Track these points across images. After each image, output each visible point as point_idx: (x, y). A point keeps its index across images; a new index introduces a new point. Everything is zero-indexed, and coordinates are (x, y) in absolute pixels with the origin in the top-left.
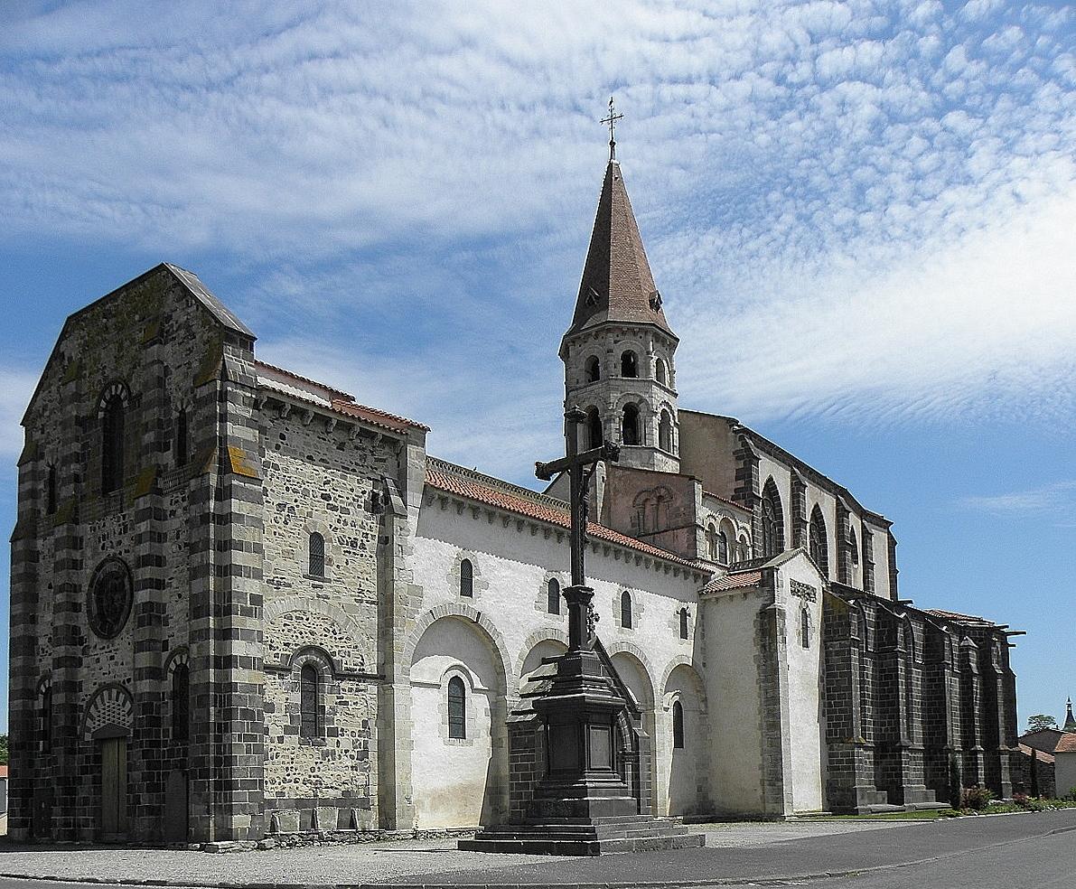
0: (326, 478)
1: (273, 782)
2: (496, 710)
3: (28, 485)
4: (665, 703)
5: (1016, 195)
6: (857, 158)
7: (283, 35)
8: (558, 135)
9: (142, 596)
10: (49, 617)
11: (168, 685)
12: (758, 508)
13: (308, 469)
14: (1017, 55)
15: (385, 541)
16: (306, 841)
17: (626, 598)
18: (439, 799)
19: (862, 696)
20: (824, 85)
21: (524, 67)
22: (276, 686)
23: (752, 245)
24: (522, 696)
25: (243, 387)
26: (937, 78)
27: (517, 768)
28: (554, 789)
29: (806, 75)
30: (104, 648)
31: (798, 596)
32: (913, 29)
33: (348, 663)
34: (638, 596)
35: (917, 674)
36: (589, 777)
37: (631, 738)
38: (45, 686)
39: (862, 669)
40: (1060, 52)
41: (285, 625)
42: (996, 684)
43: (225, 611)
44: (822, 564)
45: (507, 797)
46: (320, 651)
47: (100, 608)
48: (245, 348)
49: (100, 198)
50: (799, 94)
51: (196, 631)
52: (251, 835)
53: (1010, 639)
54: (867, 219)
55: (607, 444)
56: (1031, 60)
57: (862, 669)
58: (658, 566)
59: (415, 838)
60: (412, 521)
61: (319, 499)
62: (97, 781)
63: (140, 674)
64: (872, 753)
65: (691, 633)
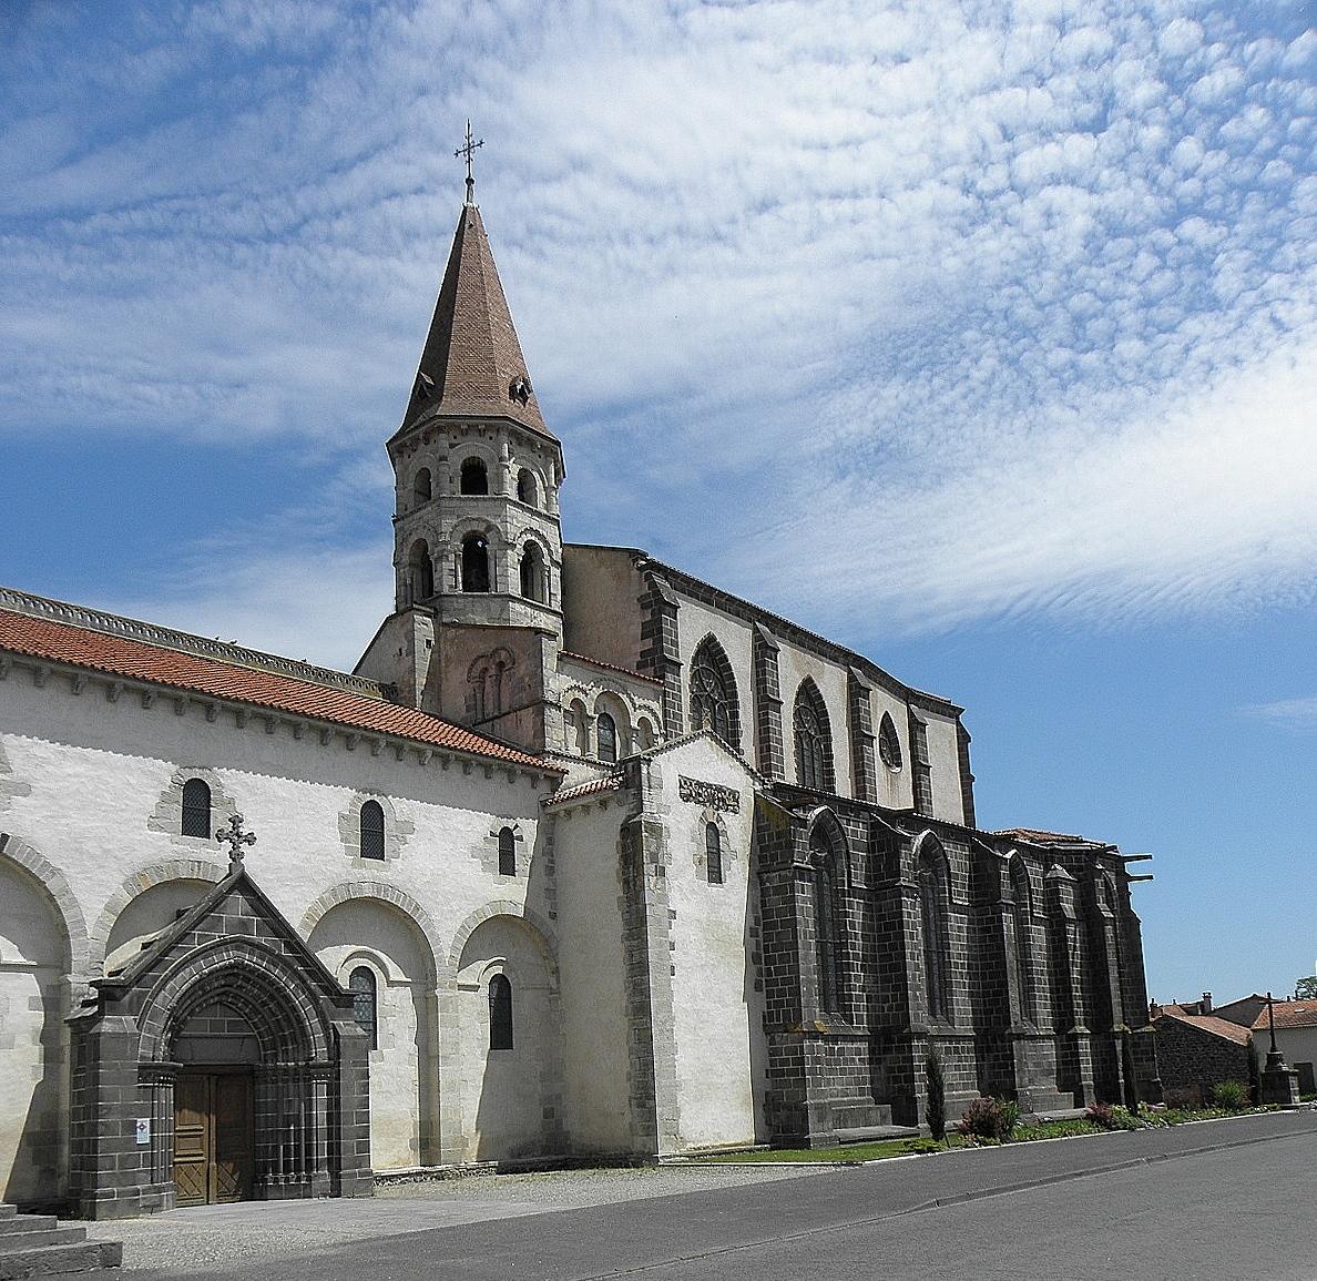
5: (1274, 320)
14: (1266, 143)
20: (1021, 191)
23: (946, 399)
26: (1166, 175)
32: (1130, 116)
34: (397, 809)
37: (327, 1037)
42: (1104, 934)
45: (66, 1149)
49: (145, 379)
50: (993, 204)
53: (1130, 868)
54: (1090, 359)
56: (1283, 148)
64: (864, 1045)
65: (522, 863)
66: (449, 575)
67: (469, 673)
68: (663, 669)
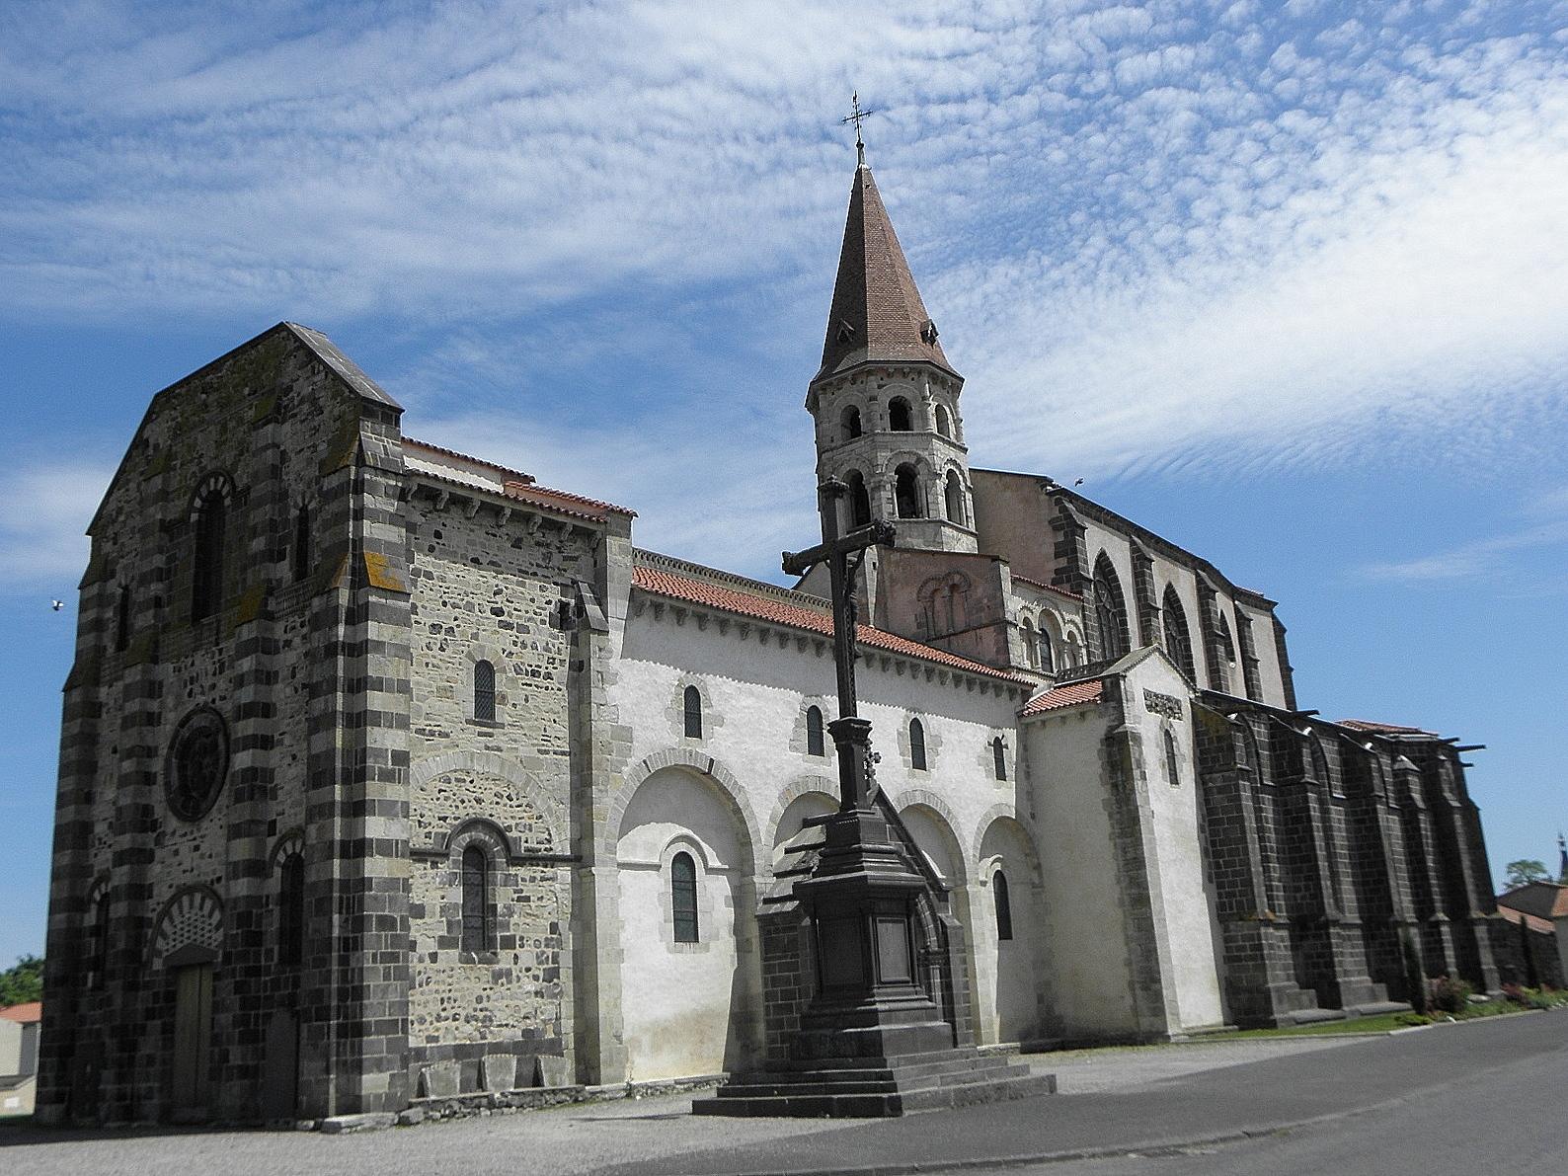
0: (497, 586)
1: (422, 1021)
2: (740, 897)
3: (91, 614)
4: (981, 873)
6: (1174, 168)
7: (471, 77)
8: (806, 166)
9: (242, 760)
10: (110, 794)
11: (274, 884)
12: (1089, 594)
13: (473, 575)
14: (1358, 49)
15: (579, 667)
16: (472, 1107)
17: (916, 728)
18: (664, 1034)
19: (1263, 849)
21: (762, 96)
22: (427, 880)
24: (778, 875)
25: (385, 473)
27: (775, 981)
28: (831, 1015)
29: (1103, 84)
30: (185, 835)
31: (1157, 712)
34: (932, 723)
35: (1337, 814)
36: (879, 995)
37: (936, 927)
38: (100, 891)
39: (1258, 810)
40: (1410, 43)
41: (440, 791)
43: (357, 775)
44: (1184, 664)
46: (490, 826)
47: (183, 777)
48: (390, 423)
49: (238, 265)
51: (315, 807)
52: (389, 1103)
53: (1464, 757)
54: (1196, 236)
55: (877, 523)
57: (1258, 810)
58: (957, 680)
59: (629, 1096)
60: (616, 638)
61: (488, 614)
62: (168, 1030)
63: (235, 871)
66: (886, 506)
67: (919, 593)
68: (1080, 585)
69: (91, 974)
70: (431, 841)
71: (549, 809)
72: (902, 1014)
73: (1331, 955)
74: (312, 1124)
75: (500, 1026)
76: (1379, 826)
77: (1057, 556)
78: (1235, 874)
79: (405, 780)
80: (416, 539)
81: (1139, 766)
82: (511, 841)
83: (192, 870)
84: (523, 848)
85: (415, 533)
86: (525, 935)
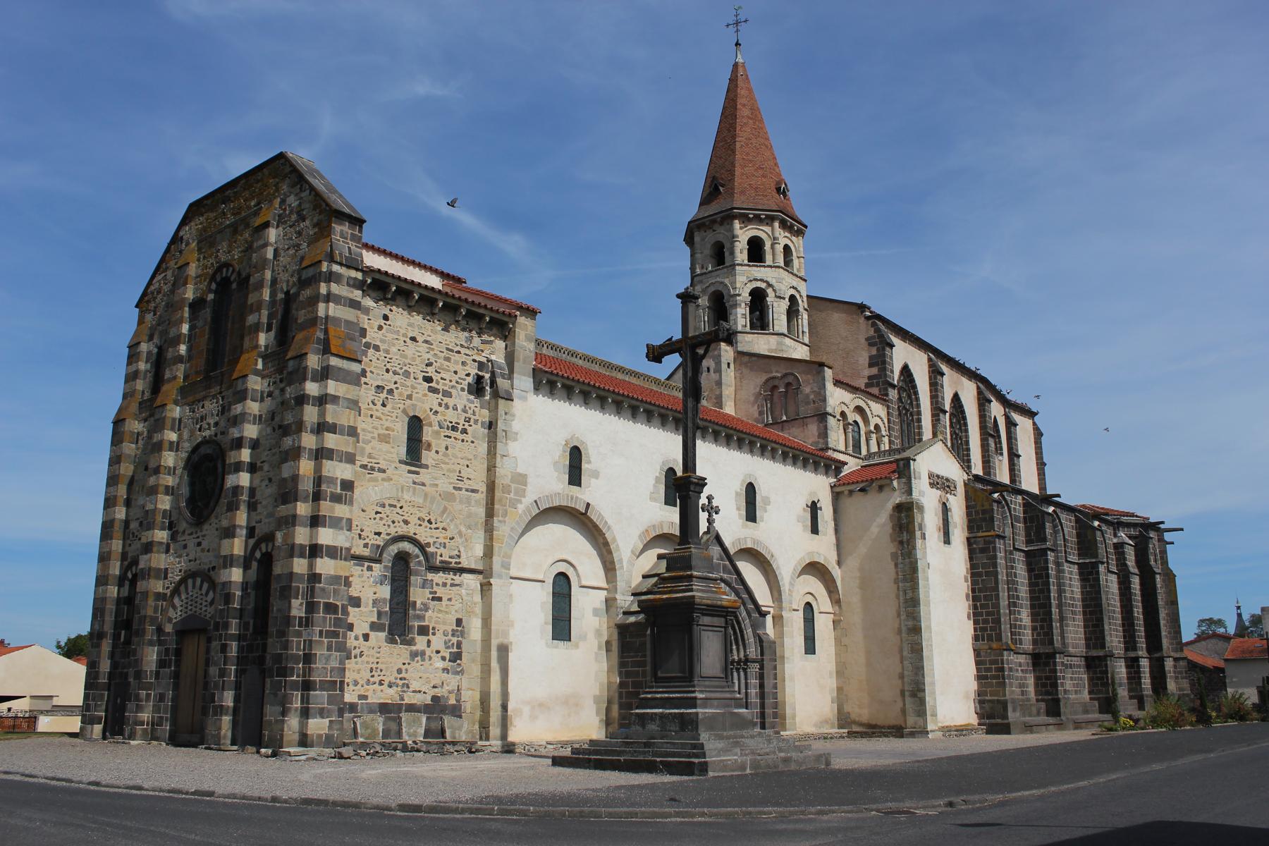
0: (428, 360)
18: (541, 706)
27: (628, 674)
31: (937, 488)
33: (444, 555)
36: (699, 686)
41: (377, 513)
52: (328, 741)
53: (1168, 537)
61: (421, 380)
69: (123, 632)
70: (368, 550)
71: (460, 533)
72: (715, 702)
73: (1056, 678)
74: (270, 751)
75: (414, 692)
76: (1099, 584)
77: (871, 365)
78: (988, 614)
79: (350, 502)
80: (369, 319)
81: (920, 529)
82: (429, 555)
83: (196, 560)
84: (438, 561)
85: (368, 314)
86: (437, 626)
